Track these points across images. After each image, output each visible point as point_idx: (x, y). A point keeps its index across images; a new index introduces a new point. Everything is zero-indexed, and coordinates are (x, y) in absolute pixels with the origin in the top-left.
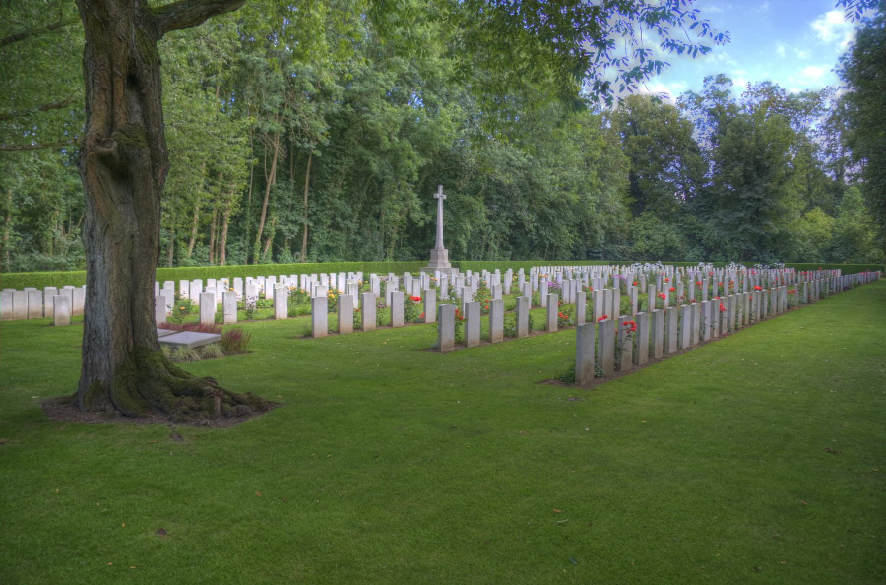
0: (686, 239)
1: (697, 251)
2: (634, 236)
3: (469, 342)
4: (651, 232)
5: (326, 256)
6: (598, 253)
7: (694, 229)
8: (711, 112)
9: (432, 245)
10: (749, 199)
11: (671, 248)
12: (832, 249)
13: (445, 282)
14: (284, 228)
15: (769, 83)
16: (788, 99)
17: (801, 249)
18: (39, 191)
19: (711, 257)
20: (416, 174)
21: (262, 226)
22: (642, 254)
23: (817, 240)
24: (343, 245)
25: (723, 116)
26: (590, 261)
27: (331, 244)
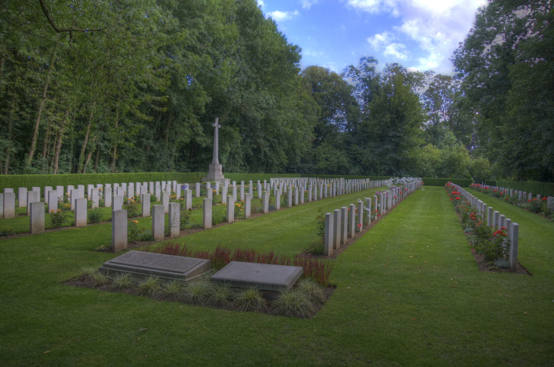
1: (357, 169)
2: (317, 158)
3: (206, 227)
4: (328, 156)
5: (131, 168)
6: (293, 169)
9: (210, 159)
11: (341, 166)
12: (441, 169)
13: (225, 189)
14: (102, 145)
16: (408, 75)
17: (425, 169)
20: (204, 108)
21: (86, 142)
22: (322, 170)
23: (434, 163)
24: (143, 159)
25: (371, 84)
26: (289, 174)
27: (135, 159)
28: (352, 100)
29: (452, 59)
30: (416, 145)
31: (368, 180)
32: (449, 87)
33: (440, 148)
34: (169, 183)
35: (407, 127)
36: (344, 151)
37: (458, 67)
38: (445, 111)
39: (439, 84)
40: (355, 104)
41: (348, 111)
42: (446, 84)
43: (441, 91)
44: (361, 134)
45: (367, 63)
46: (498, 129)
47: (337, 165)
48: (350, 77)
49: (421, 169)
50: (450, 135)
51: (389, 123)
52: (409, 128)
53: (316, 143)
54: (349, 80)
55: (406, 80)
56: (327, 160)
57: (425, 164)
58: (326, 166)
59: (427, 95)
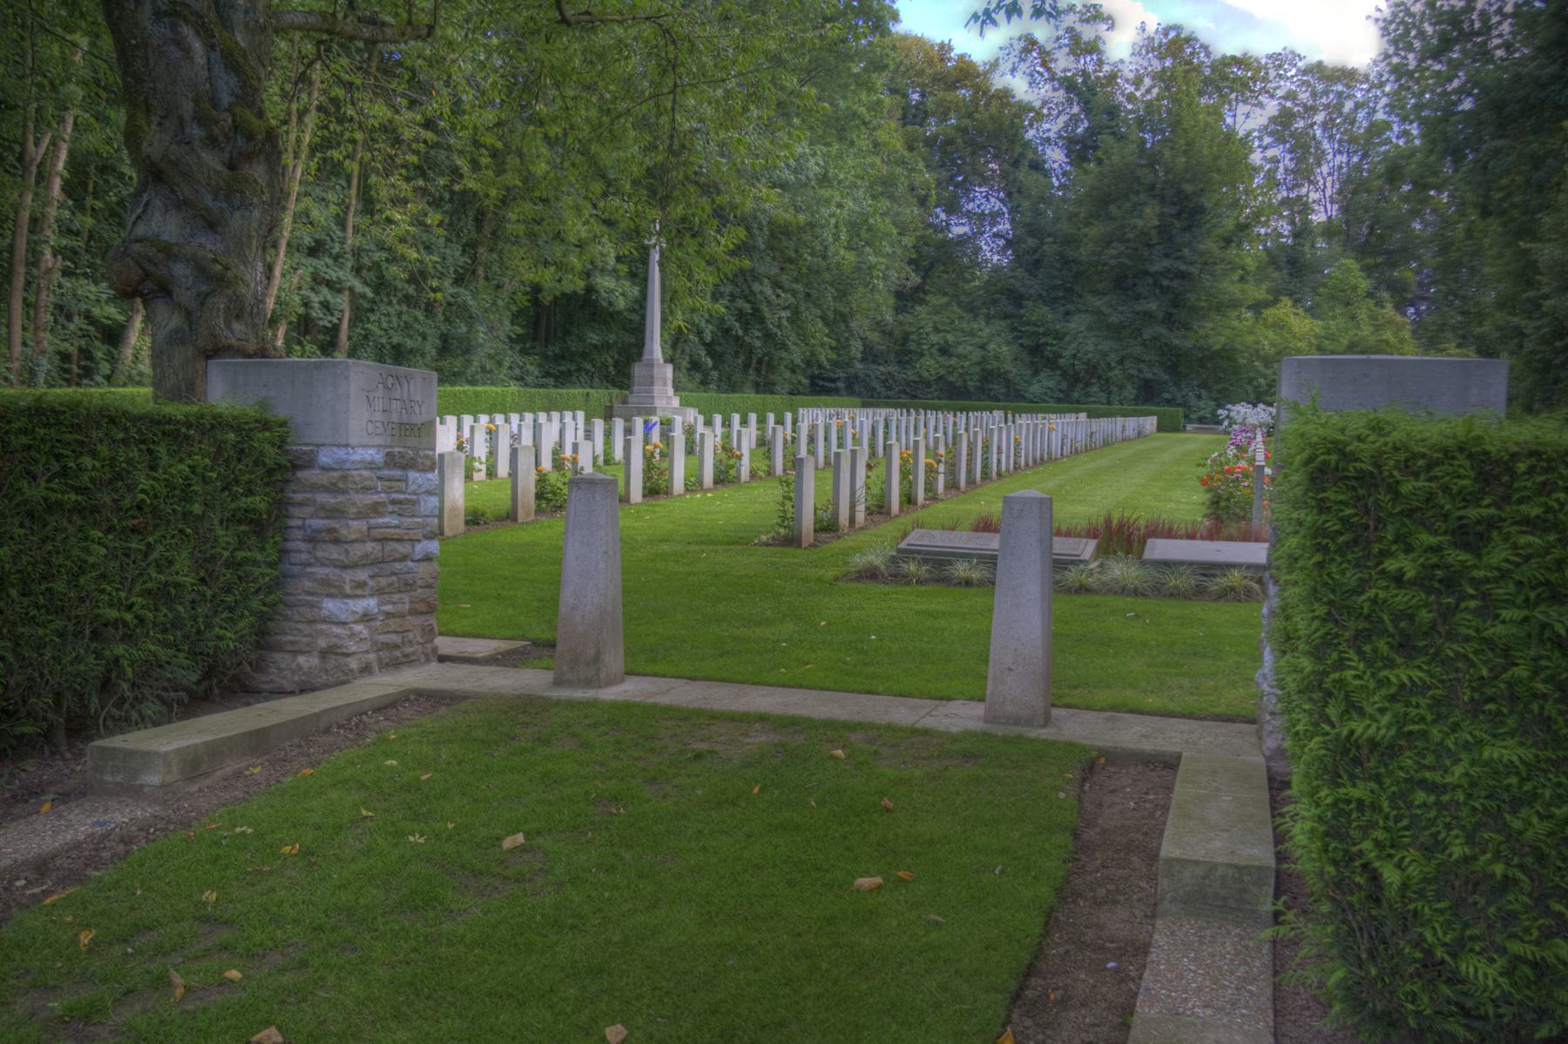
0: (1025, 357)
4: (950, 338)
7: (1044, 334)
8: (1069, 85)
9: (634, 349)
10: (1166, 273)
11: (991, 373)
14: (315, 299)
15: (1177, 28)
17: (1262, 381)
18: (471, 214)
19: (1076, 395)
28: (1030, 155)
29: (1378, 15)
30: (1235, 304)
31: (1083, 416)
32: (1348, 106)
33: (1313, 312)
34: (529, 416)
35: (1210, 245)
36: (1001, 325)
37: (1395, 42)
38: (1328, 192)
39: (1314, 95)
40: (1037, 166)
41: (1013, 191)
42: (1339, 95)
43: (1320, 117)
44: (1051, 266)
45: (1079, 27)
46: (1526, 251)
47: (977, 369)
48: (1018, 75)
49: (1250, 381)
50: (1349, 270)
51: (1153, 232)
52: (1217, 252)
53: (906, 299)
54: (1019, 86)
55: (1207, 82)
56: (944, 351)
57: (1266, 366)
58: (942, 372)
59: (1271, 134)
